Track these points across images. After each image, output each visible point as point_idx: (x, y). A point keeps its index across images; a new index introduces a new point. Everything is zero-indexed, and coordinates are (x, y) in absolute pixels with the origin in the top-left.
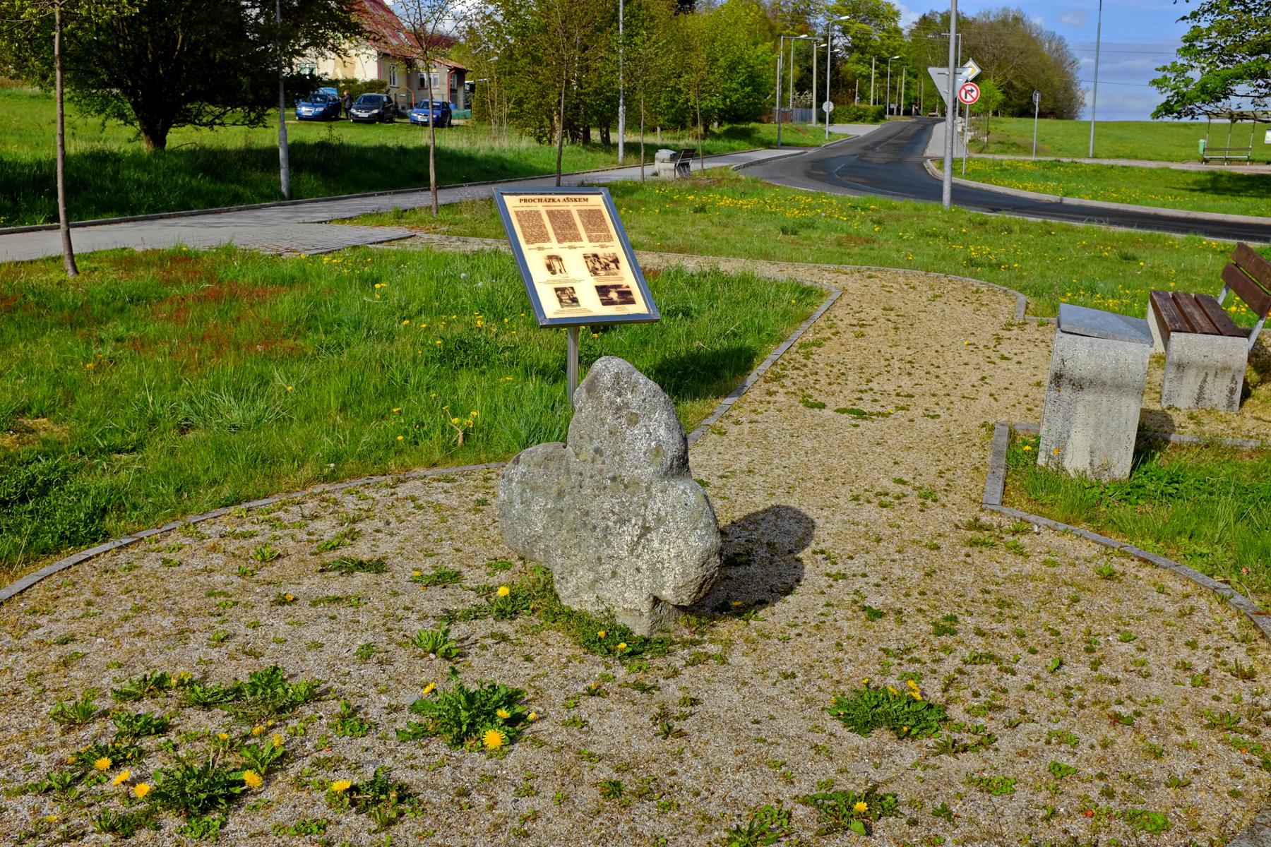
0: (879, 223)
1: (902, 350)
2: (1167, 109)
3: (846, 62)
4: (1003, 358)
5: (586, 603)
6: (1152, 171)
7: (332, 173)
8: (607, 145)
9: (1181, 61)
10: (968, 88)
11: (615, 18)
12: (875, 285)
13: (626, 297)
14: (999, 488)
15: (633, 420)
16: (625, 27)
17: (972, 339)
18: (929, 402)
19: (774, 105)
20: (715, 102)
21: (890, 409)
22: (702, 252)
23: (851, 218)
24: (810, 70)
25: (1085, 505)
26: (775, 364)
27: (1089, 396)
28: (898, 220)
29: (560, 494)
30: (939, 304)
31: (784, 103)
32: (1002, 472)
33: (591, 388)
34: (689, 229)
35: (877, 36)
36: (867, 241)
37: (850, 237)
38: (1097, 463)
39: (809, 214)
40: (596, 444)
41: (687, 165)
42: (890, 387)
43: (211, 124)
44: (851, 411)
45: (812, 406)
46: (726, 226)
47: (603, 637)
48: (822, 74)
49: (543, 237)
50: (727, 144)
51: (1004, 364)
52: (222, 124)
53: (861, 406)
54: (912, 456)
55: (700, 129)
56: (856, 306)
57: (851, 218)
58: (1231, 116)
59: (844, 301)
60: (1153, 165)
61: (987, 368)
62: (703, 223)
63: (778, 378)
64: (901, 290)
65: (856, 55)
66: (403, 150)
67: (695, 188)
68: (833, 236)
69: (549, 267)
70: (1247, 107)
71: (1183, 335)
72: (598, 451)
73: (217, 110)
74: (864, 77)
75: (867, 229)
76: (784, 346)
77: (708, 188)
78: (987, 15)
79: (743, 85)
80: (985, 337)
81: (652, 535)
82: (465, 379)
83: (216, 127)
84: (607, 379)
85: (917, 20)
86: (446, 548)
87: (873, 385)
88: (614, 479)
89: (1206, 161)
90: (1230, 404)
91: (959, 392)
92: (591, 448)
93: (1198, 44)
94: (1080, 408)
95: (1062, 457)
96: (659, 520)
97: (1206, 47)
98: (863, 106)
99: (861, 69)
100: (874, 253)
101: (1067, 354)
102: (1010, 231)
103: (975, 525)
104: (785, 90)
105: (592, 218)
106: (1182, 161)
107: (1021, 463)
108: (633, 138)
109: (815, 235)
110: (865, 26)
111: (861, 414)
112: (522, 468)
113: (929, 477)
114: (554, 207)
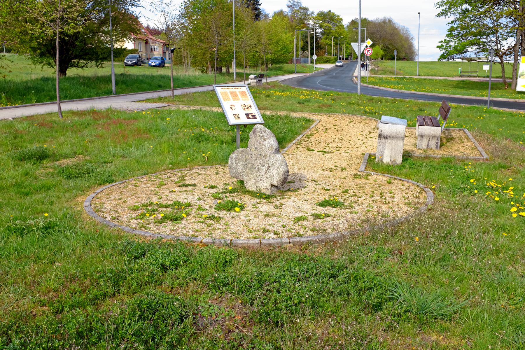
0: (334, 100)
1: (339, 136)
2: (443, 57)
3: (321, 39)
4: (371, 138)
5: (253, 188)
6: (440, 80)
7: (127, 85)
8: (228, 73)
9: (448, 39)
10: (368, 49)
11: (231, 24)
12: (331, 119)
13: (254, 117)
14: (365, 166)
15: (265, 140)
16: (235, 27)
17: (362, 133)
18: (346, 149)
19: (293, 57)
20: (270, 56)
21: (335, 151)
22: (271, 110)
23: (323, 98)
24: (307, 43)
25: (388, 169)
26: (298, 140)
27: (389, 141)
28: (341, 99)
29: (246, 160)
30: (352, 124)
31: (297, 56)
32: (366, 164)
33: (254, 132)
34: (265, 103)
35: (334, 29)
36: (329, 106)
37: (323, 105)
38: (392, 160)
39: (308, 97)
40: (256, 146)
41: (261, 80)
42: (335, 146)
43: (82, 67)
44: (322, 152)
45: (310, 151)
46: (278, 102)
47: (258, 195)
48: (312, 44)
49: (228, 99)
50: (275, 72)
51: (371, 139)
52: (87, 67)
53: (325, 150)
54: (340, 161)
55: (264, 66)
56: (324, 125)
57: (323, 98)
58: (467, 59)
59: (320, 123)
60: (441, 78)
61: (365, 141)
62: (269, 101)
63: (299, 144)
64: (340, 120)
65: (325, 36)
66: (153, 77)
67: (265, 88)
68: (317, 105)
69: (231, 108)
70: (473, 56)
71: (422, 127)
72: (256, 148)
73: (85, 62)
74: (329, 45)
75: (329, 102)
76: (301, 136)
77: (269, 89)
78: (377, 19)
79: (282, 50)
80: (366, 132)
81: (271, 168)
82: (203, 145)
83: (84, 68)
84: (258, 130)
85: (350, 22)
86: (211, 181)
87: (330, 145)
88: (260, 155)
89: (461, 76)
90: (437, 148)
91: (356, 146)
92: (254, 147)
93: (453, 33)
94: (387, 144)
95: (382, 159)
96: (272, 164)
97: (456, 34)
98: (329, 56)
99: (328, 42)
100: (331, 110)
101: (382, 129)
102: (381, 102)
103: (356, 174)
104: (297, 50)
105: (243, 93)
106: (453, 76)
107: (372, 162)
108: (239, 71)
109: (310, 104)
110: (329, 25)
111: (325, 152)
112: (235, 155)
113: (344, 165)
114: (231, 90)
